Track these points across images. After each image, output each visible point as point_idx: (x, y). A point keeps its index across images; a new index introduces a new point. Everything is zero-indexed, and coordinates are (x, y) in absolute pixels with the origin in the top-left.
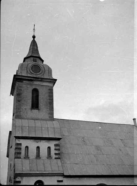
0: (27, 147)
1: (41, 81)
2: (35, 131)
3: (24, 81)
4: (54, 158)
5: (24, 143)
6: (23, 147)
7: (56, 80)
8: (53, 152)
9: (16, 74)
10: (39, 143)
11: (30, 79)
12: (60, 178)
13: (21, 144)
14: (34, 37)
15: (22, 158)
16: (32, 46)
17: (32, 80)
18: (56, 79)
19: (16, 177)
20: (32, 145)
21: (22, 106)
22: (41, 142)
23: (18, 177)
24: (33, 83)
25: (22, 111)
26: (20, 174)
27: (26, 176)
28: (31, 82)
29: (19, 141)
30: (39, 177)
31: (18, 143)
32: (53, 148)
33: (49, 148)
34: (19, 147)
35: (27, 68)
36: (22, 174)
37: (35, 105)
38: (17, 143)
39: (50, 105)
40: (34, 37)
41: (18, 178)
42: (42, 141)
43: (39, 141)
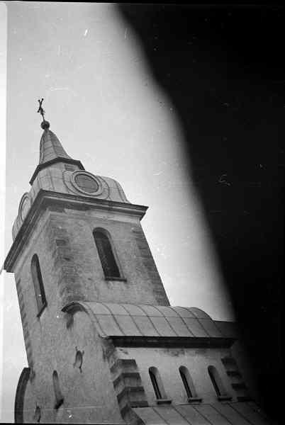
0: (152, 372)
1: (109, 210)
3: (66, 210)
5: (144, 359)
9: (50, 129)
10: (180, 355)
11: (82, 202)
13: (133, 363)
14: (45, 125)
15: (149, 404)
17: (86, 208)
18: (145, 205)
21: (80, 272)
24: (89, 214)
25: (82, 283)
28: (86, 213)
29: (126, 353)
31: (124, 358)
34: (131, 370)
35: (63, 178)
37: (112, 272)
38: (123, 361)
40: (45, 125)
42: (185, 350)
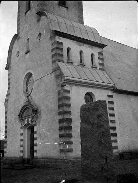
2: (74, 30)
4: (98, 68)
5: (67, 43)
7: (5, 69)
8: (97, 61)
10: (82, 46)
12: (110, 93)
15: (64, 61)
16: (13, 41)
19: (64, 85)
23: (67, 85)
26: (70, 80)
27: (76, 85)
32: (96, 56)
33: (92, 55)
36: (94, 84)
38: (58, 41)
39: (79, 5)
41: (67, 86)
43: (81, 44)
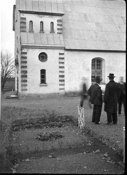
5: (29, 18)
6: (28, 21)
20: (36, 20)
22: (45, 17)
23: (24, 49)
30: (42, 50)
41: (25, 50)
